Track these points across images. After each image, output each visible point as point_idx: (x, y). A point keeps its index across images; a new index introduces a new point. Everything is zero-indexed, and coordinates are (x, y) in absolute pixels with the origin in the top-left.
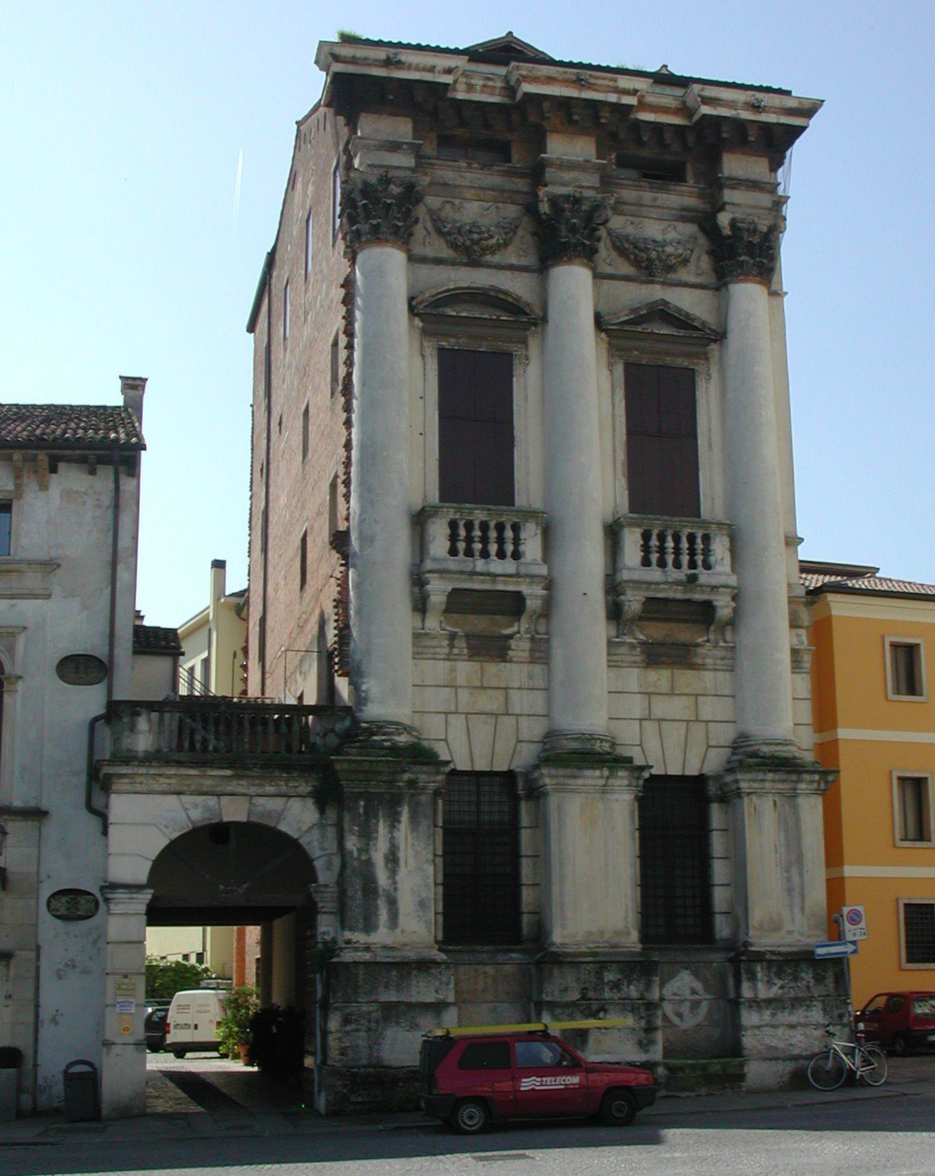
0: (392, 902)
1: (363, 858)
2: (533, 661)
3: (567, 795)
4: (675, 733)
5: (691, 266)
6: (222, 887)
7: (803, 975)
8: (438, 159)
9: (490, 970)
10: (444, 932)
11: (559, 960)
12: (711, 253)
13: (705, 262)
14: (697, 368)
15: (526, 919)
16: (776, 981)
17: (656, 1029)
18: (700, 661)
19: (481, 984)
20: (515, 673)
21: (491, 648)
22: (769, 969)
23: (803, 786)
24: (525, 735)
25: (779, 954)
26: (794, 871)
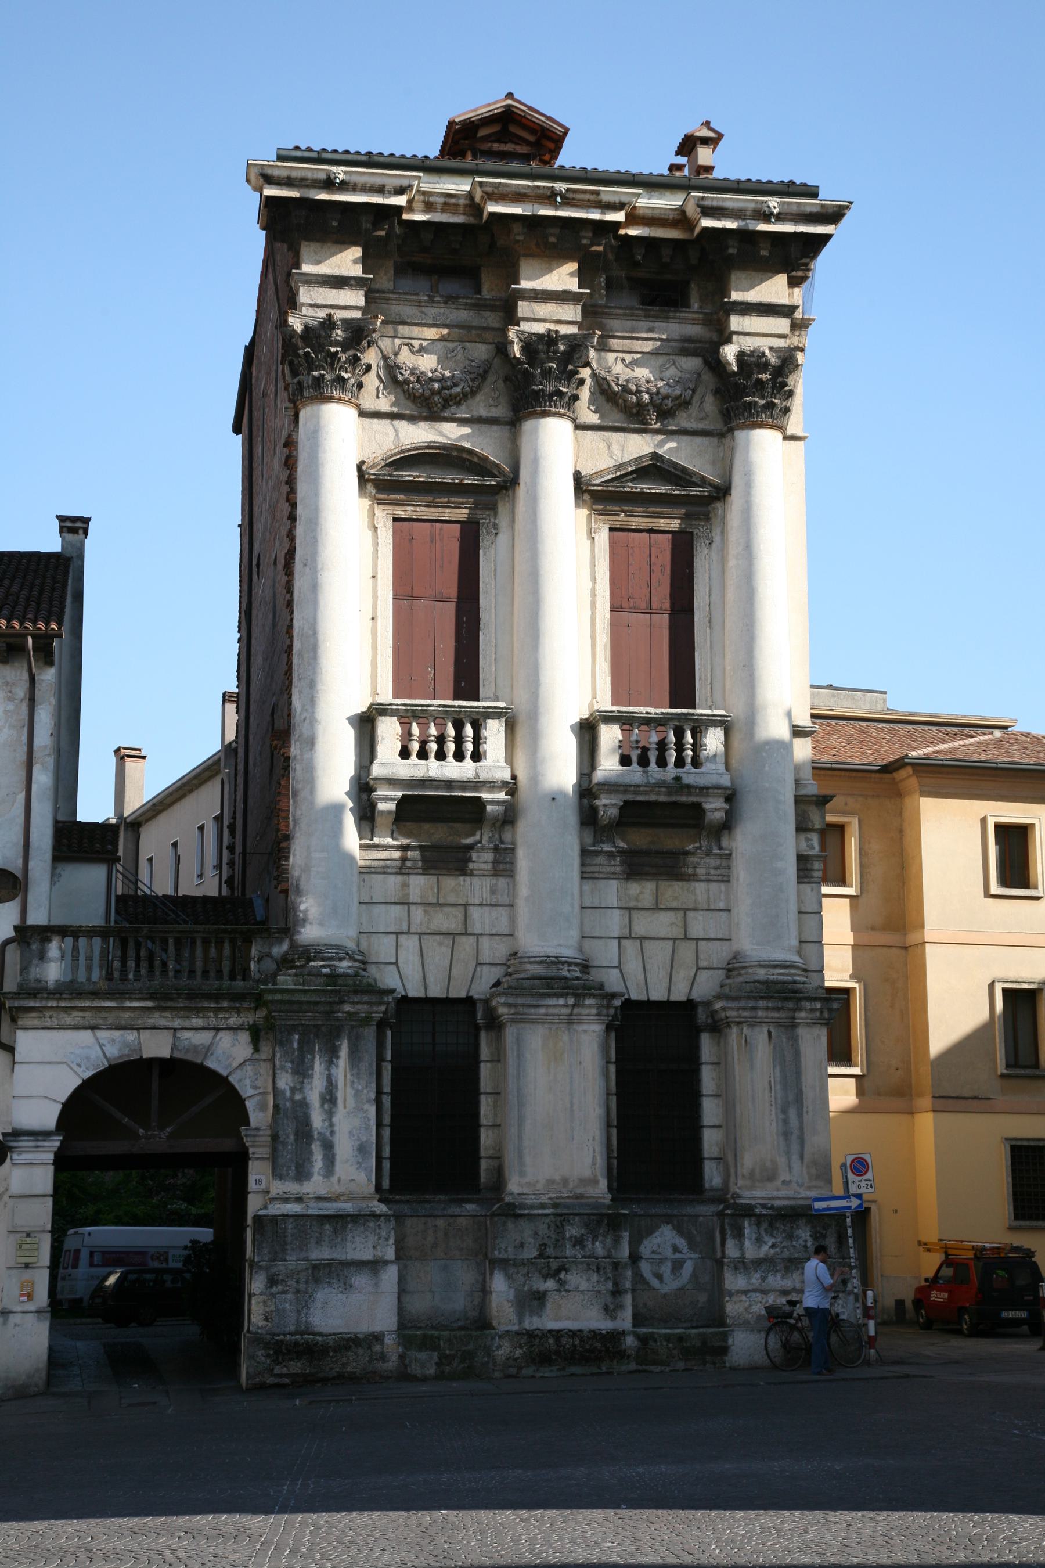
0: (328, 1147)
1: (298, 1097)
2: (496, 873)
3: (527, 1025)
4: (658, 953)
5: (693, 410)
6: (141, 1131)
7: (800, 1232)
8: (393, 293)
9: (440, 1222)
10: (391, 1180)
11: (513, 1212)
12: (717, 392)
13: (710, 404)
14: (696, 531)
15: (484, 1164)
16: (766, 1239)
17: (625, 1292)
18: (690, 871)
19: (430, 1239)
20: (477, 887)
21: (446, 860)
22: (758, 1224)
23: (803, 1014)
24: (486, 957)
25: (772, 1208)
26: (792, 1113)
